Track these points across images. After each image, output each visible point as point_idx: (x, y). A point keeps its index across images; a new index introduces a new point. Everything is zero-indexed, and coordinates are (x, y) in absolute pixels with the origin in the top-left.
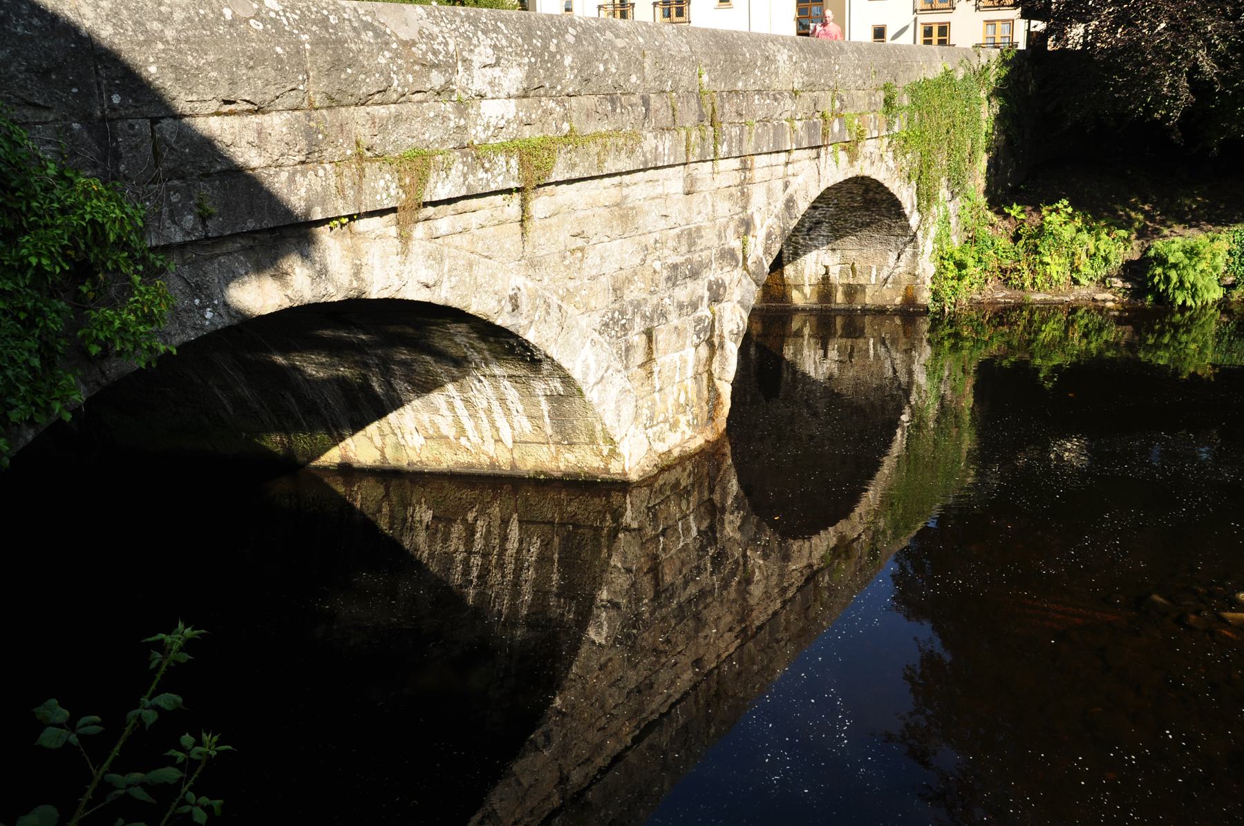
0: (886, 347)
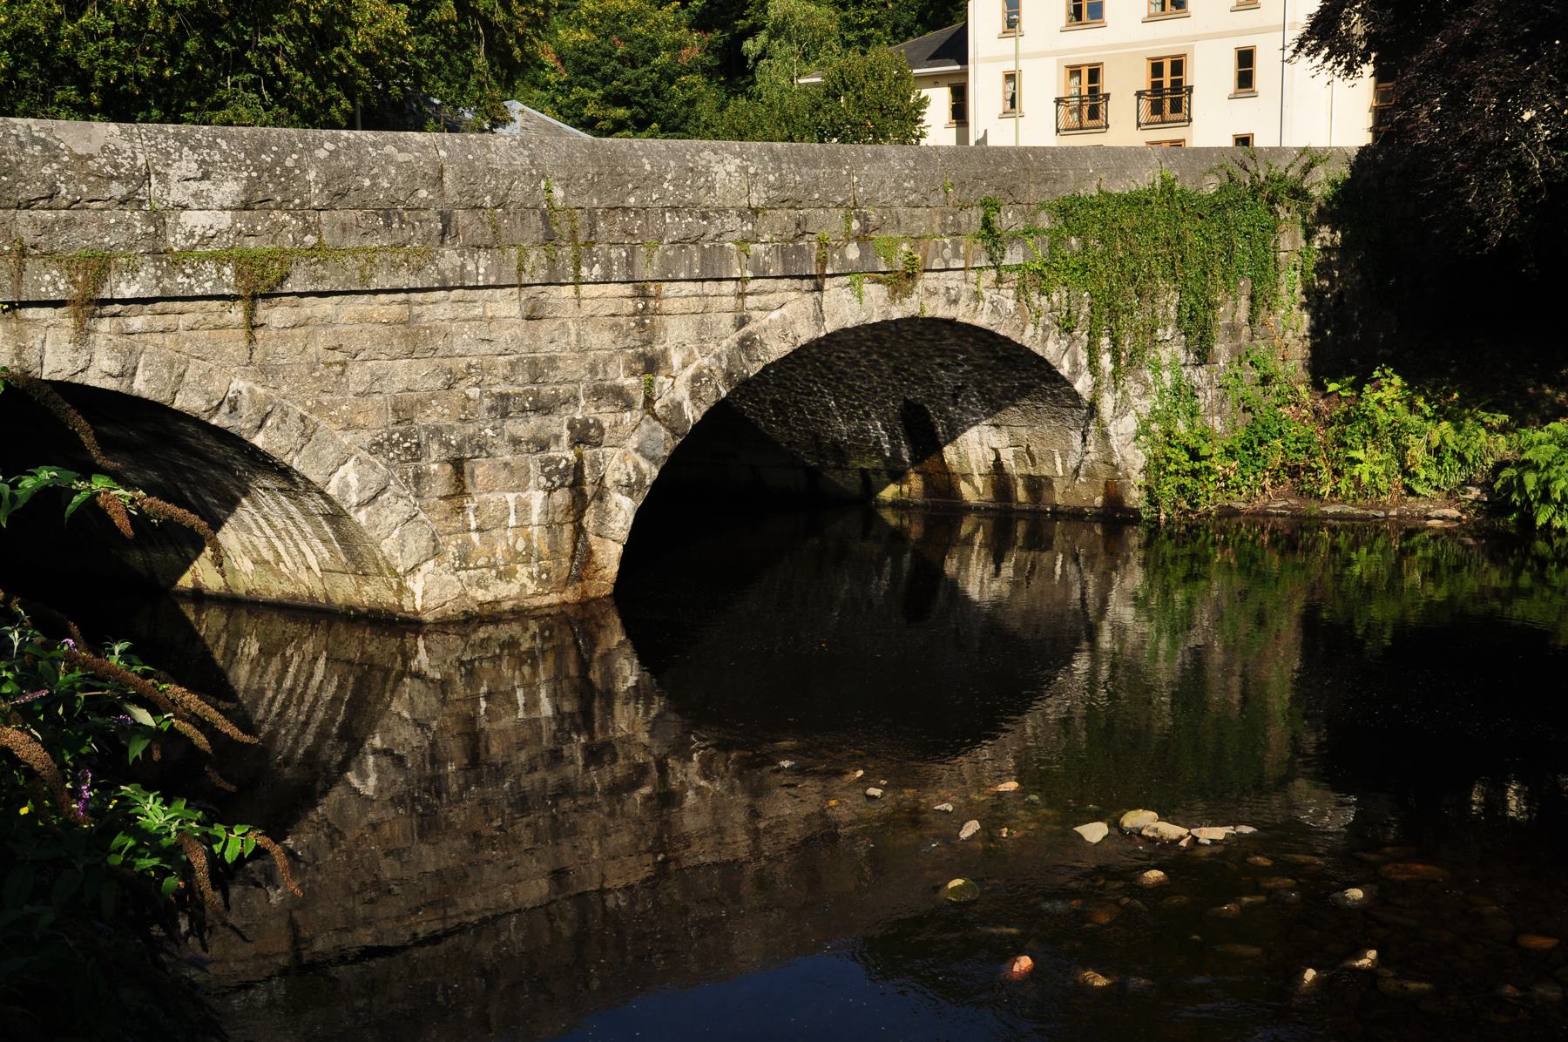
0: (1078, 565)
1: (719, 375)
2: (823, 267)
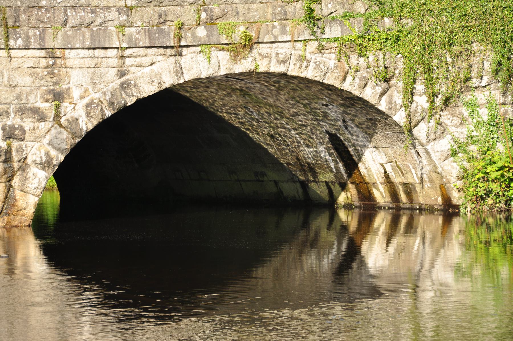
1: (105, 103)
2: (180, 40)
